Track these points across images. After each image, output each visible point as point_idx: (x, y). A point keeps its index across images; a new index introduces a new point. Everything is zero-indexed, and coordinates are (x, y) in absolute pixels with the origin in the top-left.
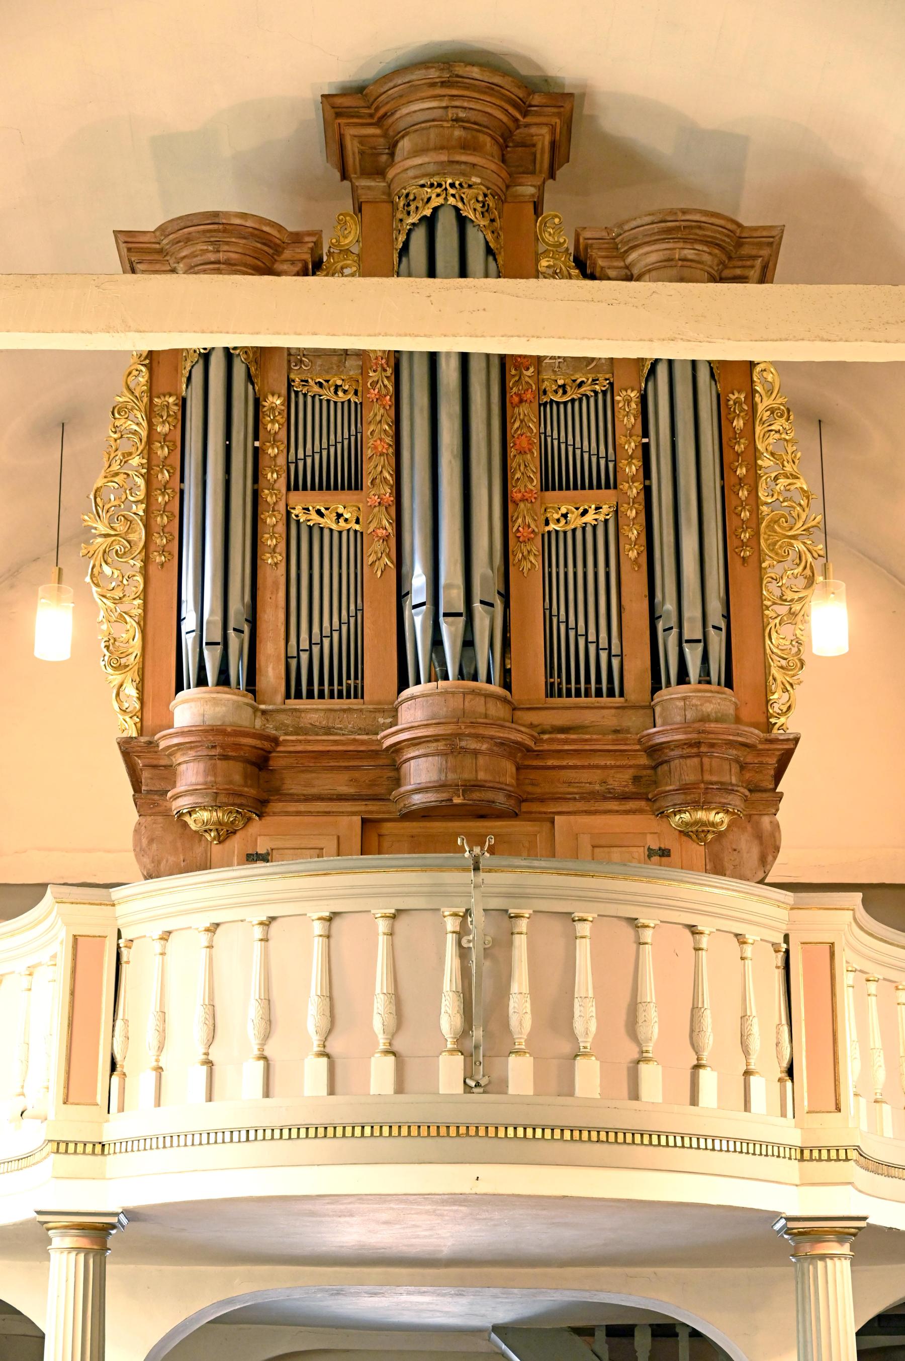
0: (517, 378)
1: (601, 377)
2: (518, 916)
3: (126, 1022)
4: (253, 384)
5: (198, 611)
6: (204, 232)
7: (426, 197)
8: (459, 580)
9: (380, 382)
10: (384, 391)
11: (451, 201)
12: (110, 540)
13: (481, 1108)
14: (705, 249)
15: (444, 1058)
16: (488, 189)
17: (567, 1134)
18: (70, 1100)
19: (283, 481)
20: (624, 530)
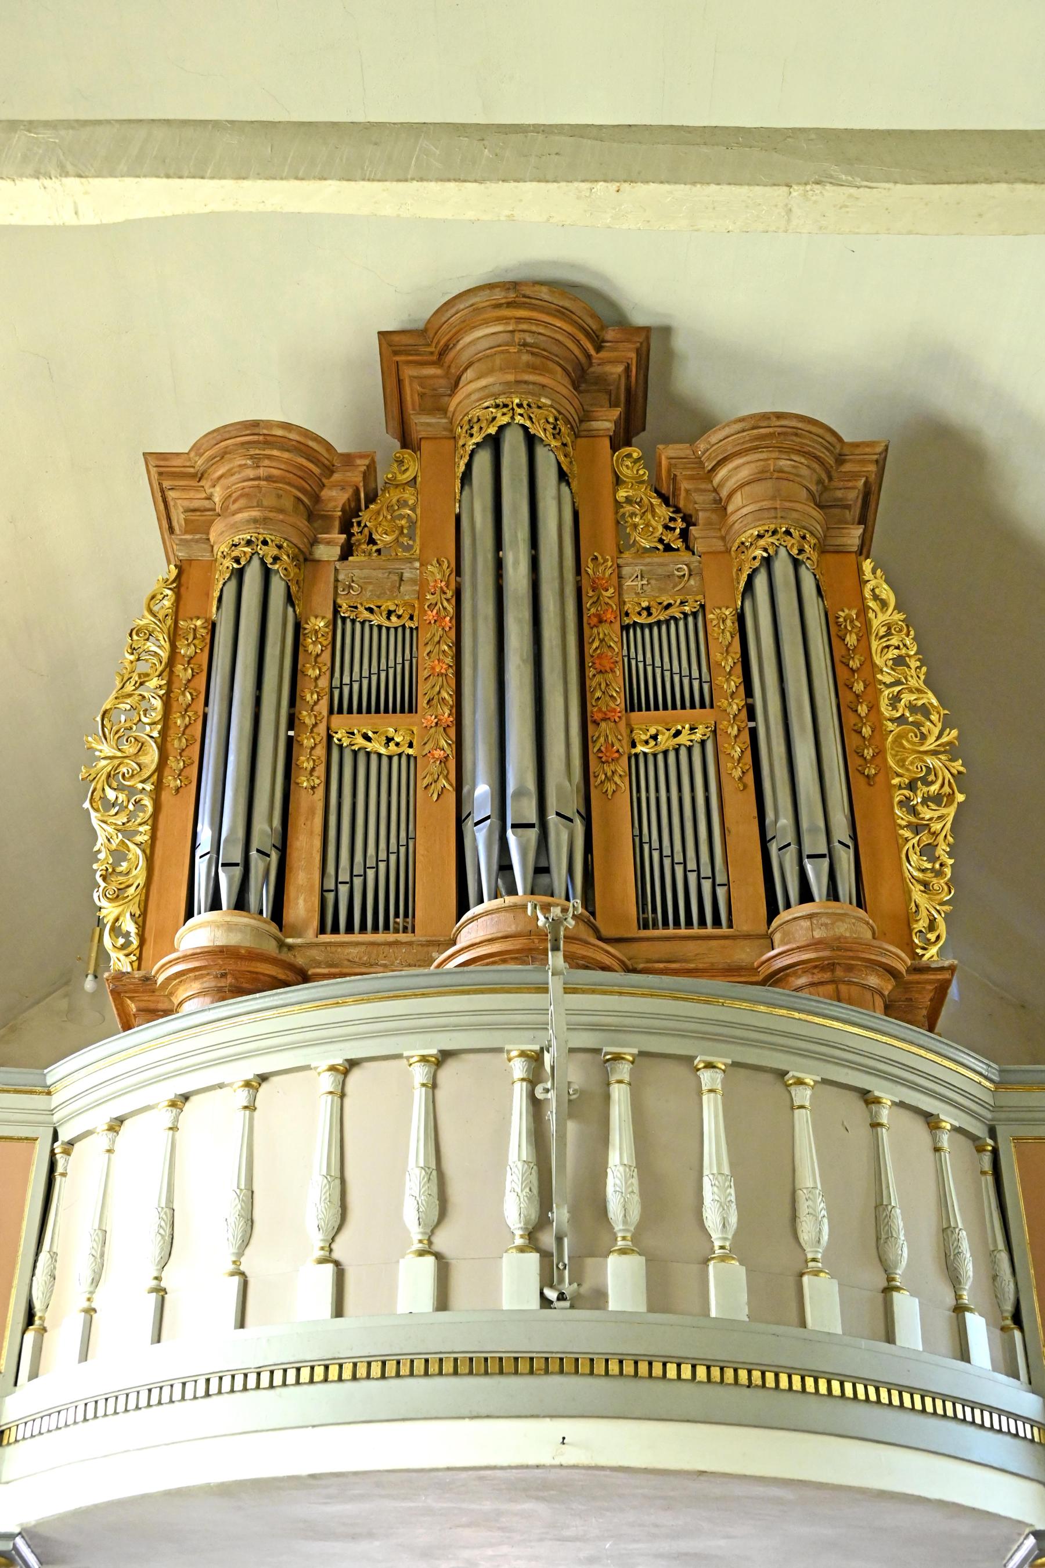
0: (595, 599)
1: (690, 599)
2: (618, 1058)
3: (54, 1256)
6: (243, 444)
7: (490, 418)
8: (531, 785)
9: (439, 605)
11: (519, 419)
12: (116, 762)
13: (568, 1332)
14: (803, 460)
16: (560, 413)
19: (324, 704)
20: (725, 746)
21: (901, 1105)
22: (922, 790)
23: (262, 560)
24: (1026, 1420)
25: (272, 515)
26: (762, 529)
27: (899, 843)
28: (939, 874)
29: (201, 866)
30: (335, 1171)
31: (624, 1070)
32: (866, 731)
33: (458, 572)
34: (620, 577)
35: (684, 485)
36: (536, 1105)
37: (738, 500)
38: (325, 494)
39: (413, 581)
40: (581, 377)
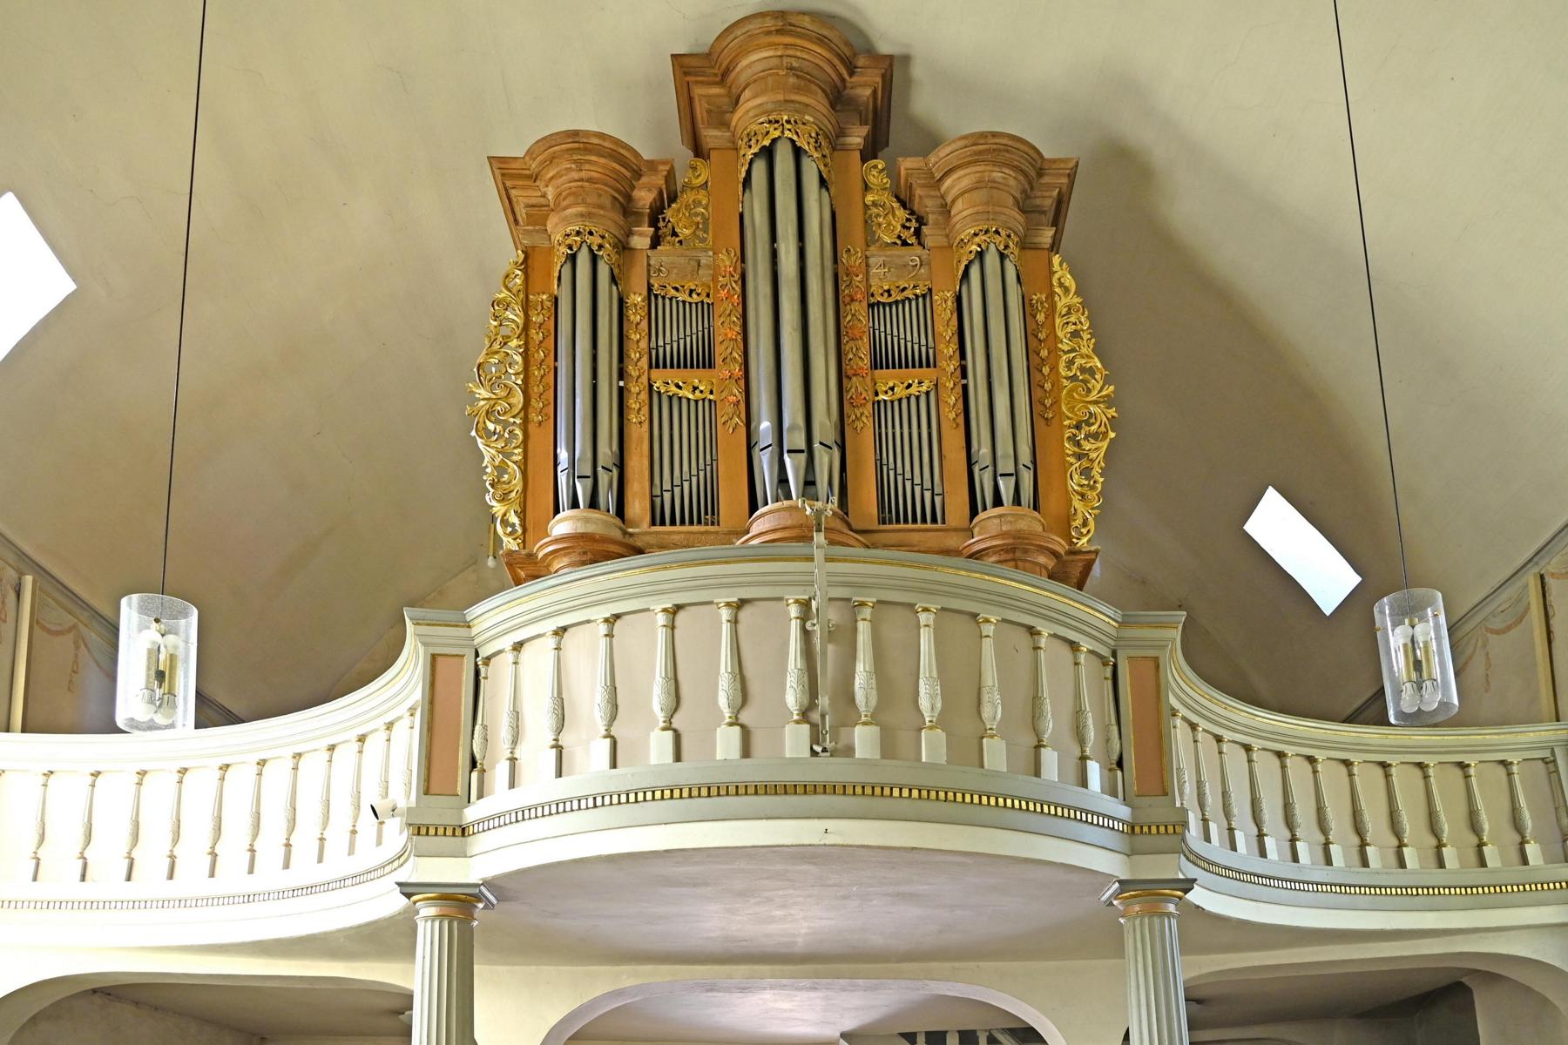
2: (862, 604)
3: (485, 727)
8: (801, 422)
11: (787, 133)
13: (829, 770)
15: (790, 729)
17: (915, 793)
18: (433, 790)
19: (645, 359)
20: (943, 395)
21: (1055, 636)
22: (1085, 429)
23: (591, 250)
24: (1119, 820)
26: (976, 229)
27: (1065, 466)
28: (1093, 488)
29: (562, 478)
30: (671, 675)
31: (867, 612)
32: (1048, 386)
33: (743, 260)
34: (867, 266)
35: (918, 192)
36: (806, 634)
37: (959, 205)
38: (637, 194)
39: (708, 267)
40: (838, 98)
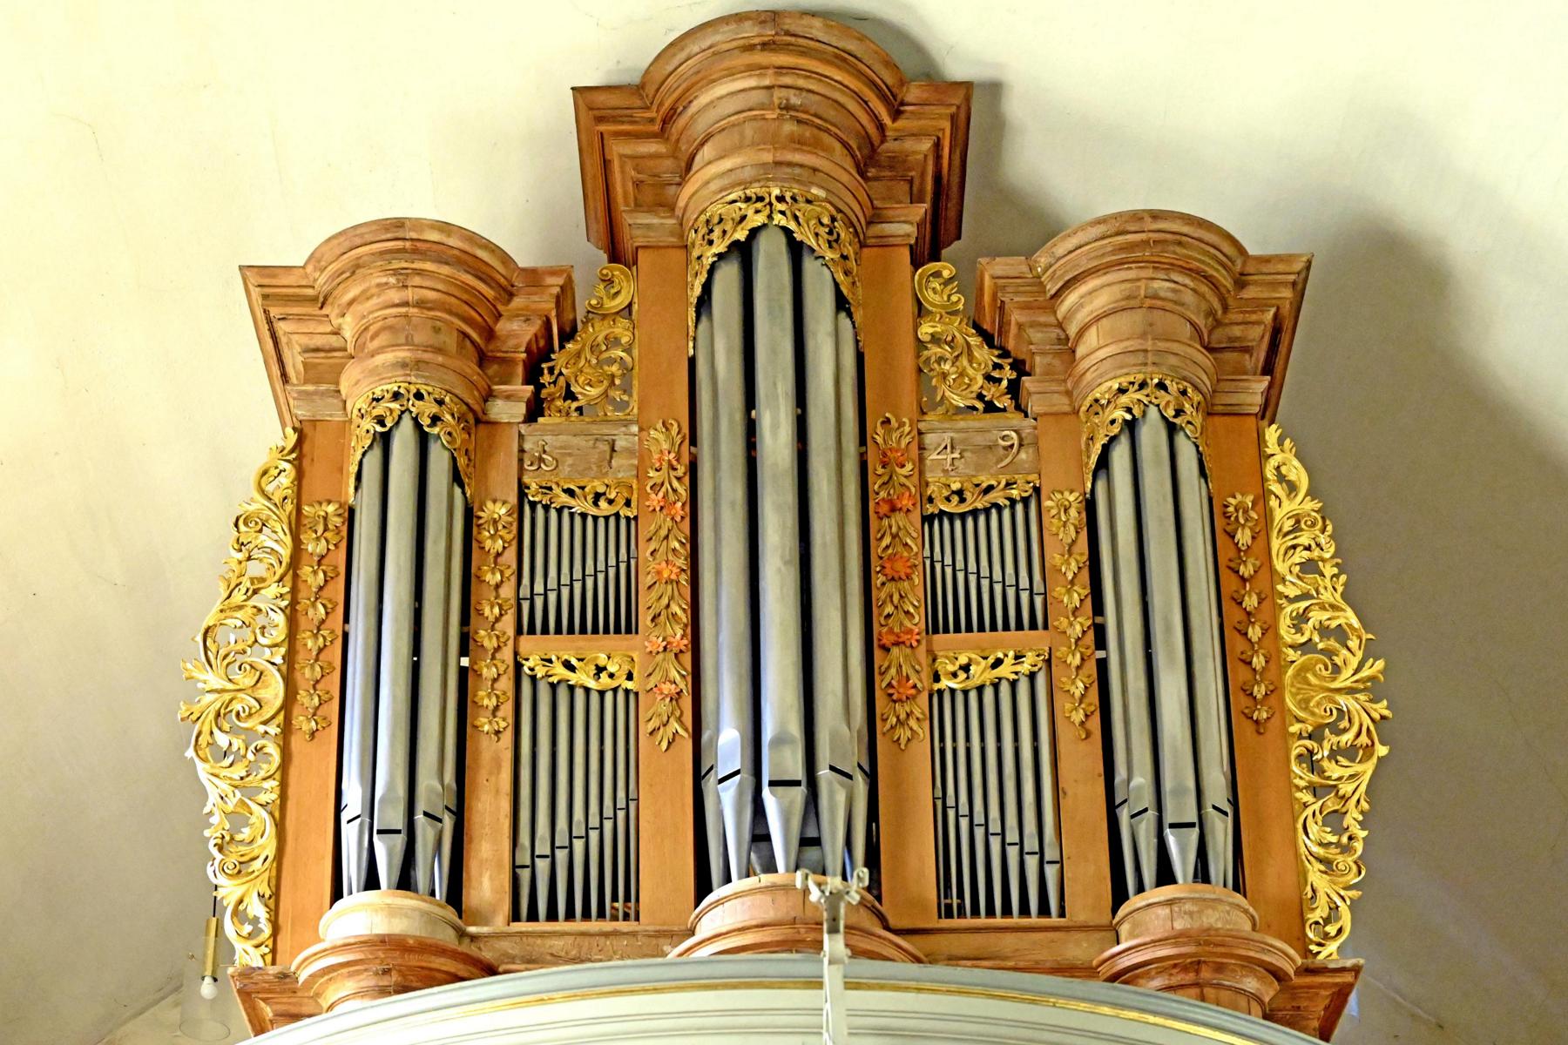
0: (886, 478)
1: (1020, 479)
4: (462, 486)
5: (371, 777)
6: (382, 253)
9: (667, 485)
10: (672, 497)
11: (778, 218)
14: (1188, 281)
25: (427, 356)
38: (502, 327)
